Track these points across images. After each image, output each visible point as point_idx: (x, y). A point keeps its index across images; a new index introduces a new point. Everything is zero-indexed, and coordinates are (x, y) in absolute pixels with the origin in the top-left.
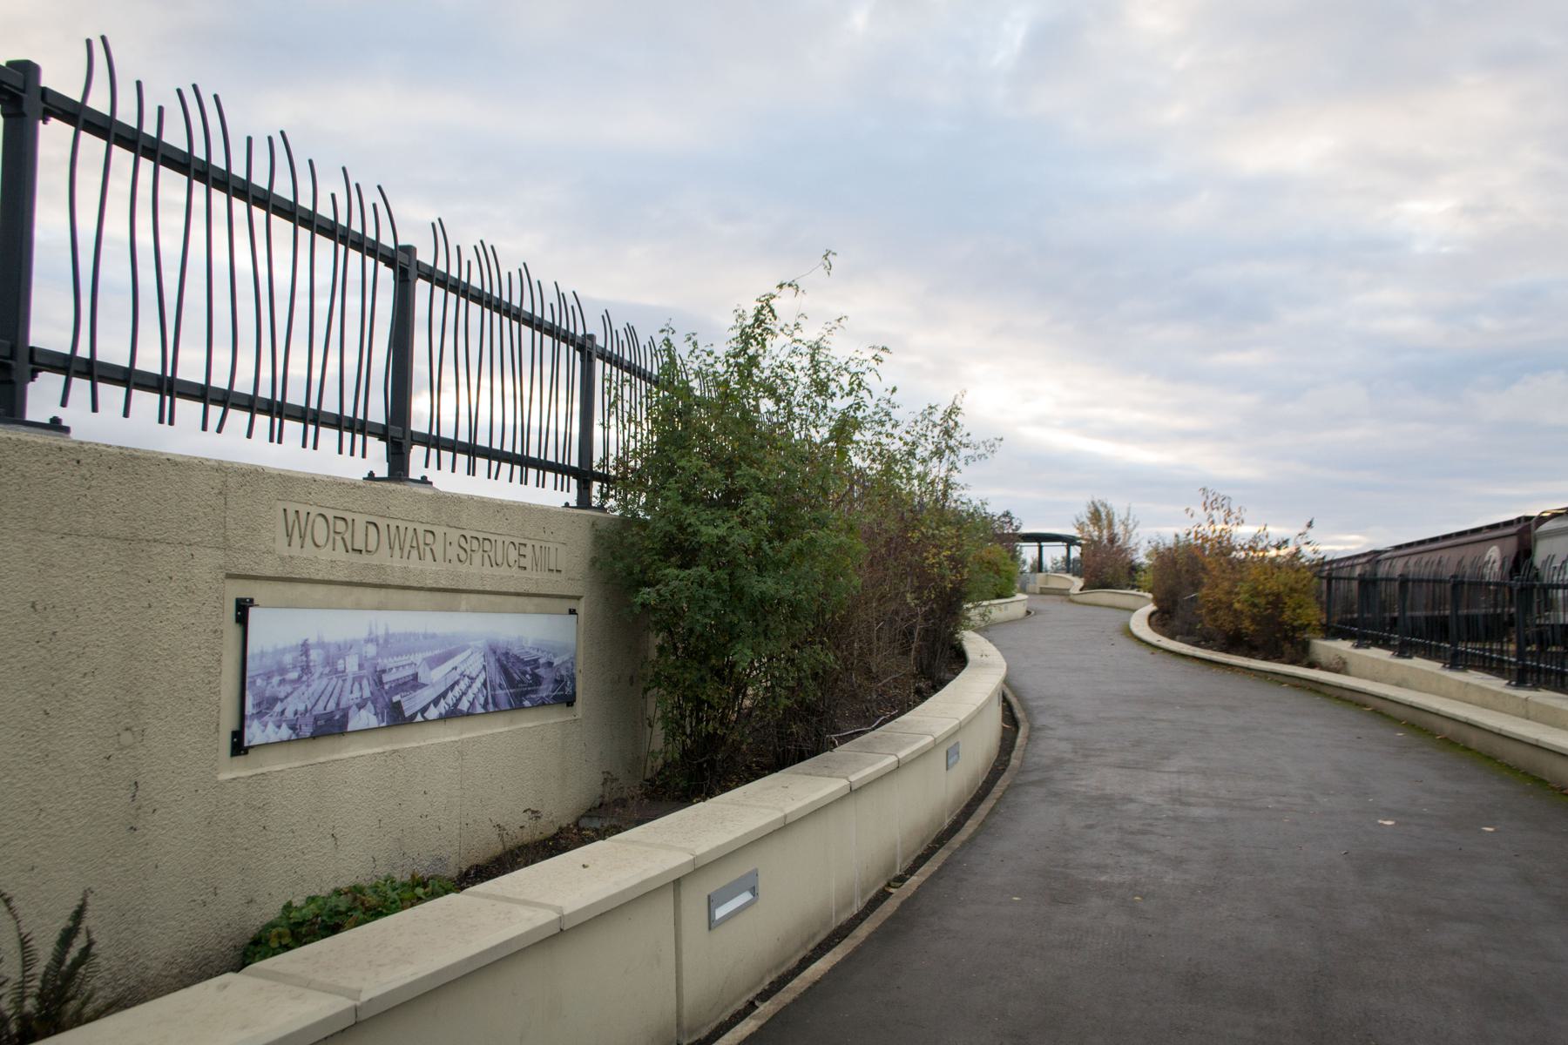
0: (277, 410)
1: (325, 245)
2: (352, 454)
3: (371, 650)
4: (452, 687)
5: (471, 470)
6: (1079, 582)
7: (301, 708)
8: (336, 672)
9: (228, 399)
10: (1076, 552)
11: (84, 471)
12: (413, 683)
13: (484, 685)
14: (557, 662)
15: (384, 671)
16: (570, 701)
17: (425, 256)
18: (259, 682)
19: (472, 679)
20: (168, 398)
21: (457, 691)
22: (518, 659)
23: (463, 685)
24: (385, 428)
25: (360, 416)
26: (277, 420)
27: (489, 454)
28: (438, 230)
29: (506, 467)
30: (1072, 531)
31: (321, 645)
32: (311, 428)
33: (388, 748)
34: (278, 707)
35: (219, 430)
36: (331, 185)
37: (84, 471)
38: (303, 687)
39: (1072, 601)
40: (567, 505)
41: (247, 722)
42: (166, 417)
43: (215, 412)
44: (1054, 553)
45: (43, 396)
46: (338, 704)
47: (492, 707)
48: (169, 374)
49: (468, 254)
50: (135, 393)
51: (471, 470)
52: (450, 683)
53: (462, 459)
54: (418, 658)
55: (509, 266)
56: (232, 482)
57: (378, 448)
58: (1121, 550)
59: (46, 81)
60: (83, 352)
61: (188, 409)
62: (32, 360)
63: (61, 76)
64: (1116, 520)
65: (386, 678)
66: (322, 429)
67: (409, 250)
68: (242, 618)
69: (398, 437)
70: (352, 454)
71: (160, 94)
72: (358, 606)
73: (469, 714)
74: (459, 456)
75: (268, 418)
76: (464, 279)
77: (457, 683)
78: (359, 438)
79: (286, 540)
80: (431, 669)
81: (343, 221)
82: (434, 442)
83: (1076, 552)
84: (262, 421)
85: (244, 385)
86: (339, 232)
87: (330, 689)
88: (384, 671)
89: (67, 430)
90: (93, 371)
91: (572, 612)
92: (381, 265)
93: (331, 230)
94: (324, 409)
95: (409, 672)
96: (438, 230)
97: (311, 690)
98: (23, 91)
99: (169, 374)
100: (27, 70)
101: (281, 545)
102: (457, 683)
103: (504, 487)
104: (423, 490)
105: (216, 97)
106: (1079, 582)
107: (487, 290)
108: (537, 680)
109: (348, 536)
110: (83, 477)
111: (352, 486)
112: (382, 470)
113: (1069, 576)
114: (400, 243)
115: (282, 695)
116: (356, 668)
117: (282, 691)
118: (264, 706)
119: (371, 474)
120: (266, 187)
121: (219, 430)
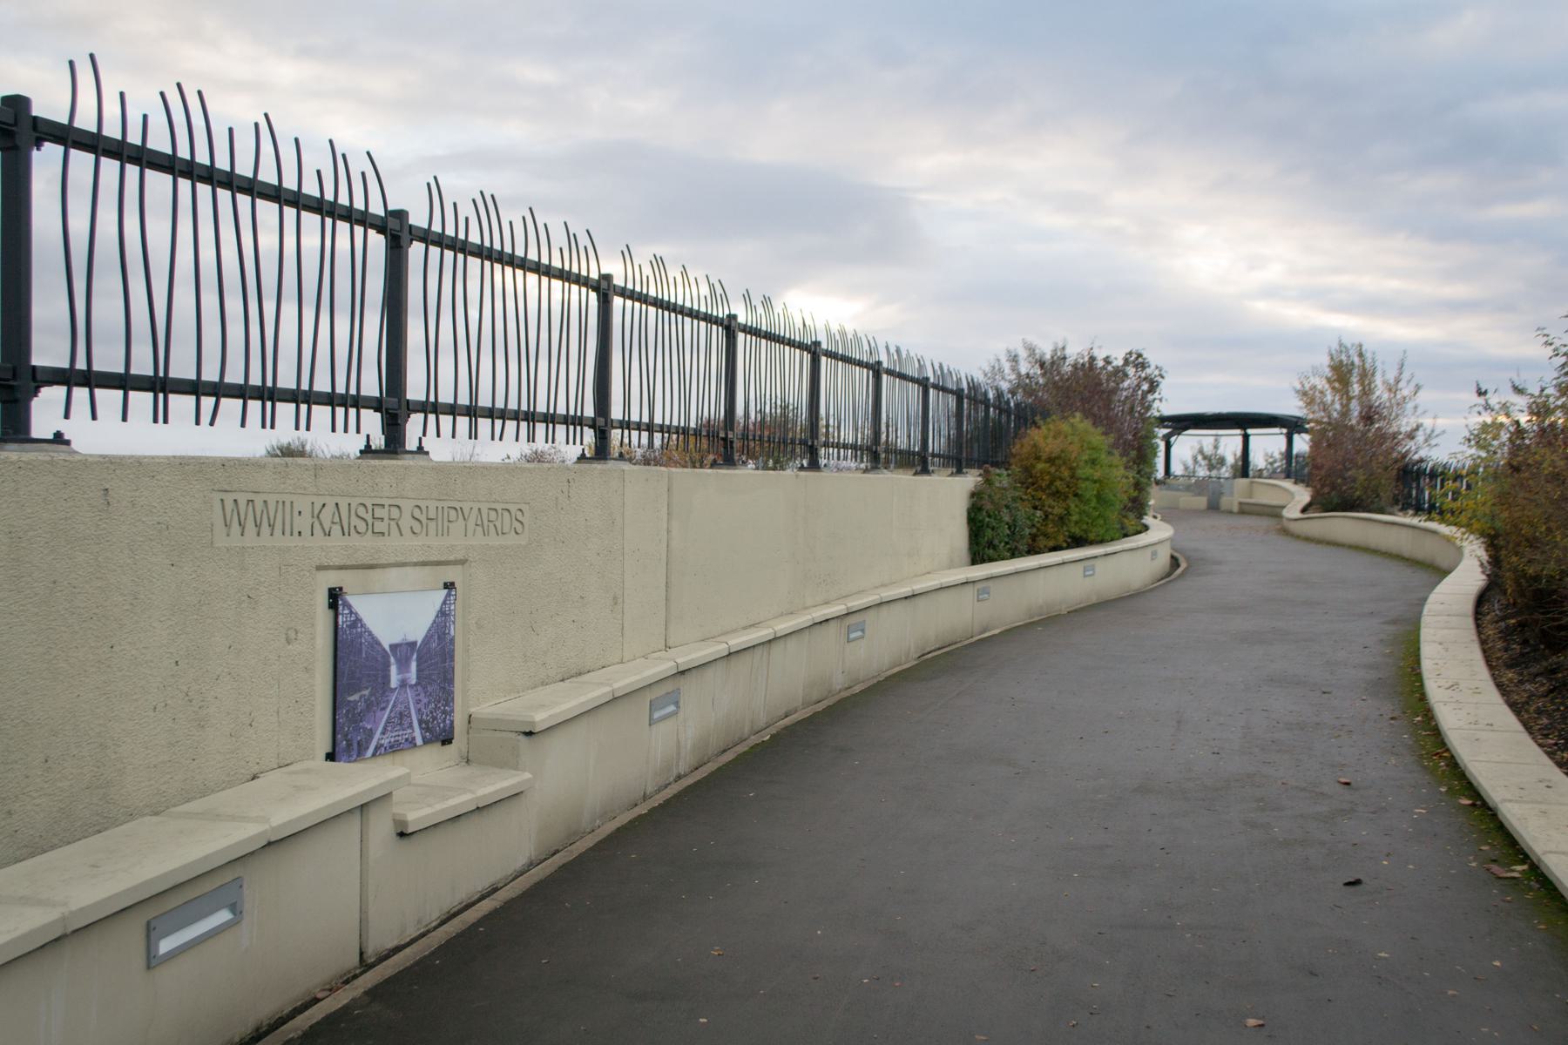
0: (269, 395)
1: (311, 220)
2: (346, 431)
5: (473, 434)
6: (1303, 495)
10: (1302, 444)
17: (418, 219)
20: (161, 396)
24: (594, 420)
25: (432, 399)
27: (491, 413)
28: (434, 190)
29: (511, 425)
30: (1292, 407)
32: (304, 407)
35: (212, 424)
36: (316, 159)
39: (1285, 532)
43: (208, 402)
44: (1267, 446)
45: (46, 411)
48: (161, 374)
49: (466, 210)
50: (132, 394)
51: (473, 434)
53: (463, 422)
55: (512, 214)
57: (372, 422)
58: (1382, 437)
59: (37, 111)
60: (81, 365)
62: (34, 378)
63: (49, 105)
64: (1378, 380)
66: (314, 407)
67: (401, 215)
70: (346, 431)
74: (459, 418)
75: (259, 403)
76: (462, 236)
78: (352, 411)
79: (255, 530)
81: (329, 196)
82: (431, 408)
83: (1302, 444)
84: (254, 406)
85: (234, 377)
86: (326, 208)
89: (68, 443)
92: (372, 233)
93: (319, 207)
94: (363, 393)
96: (434, 190)
98: (15, 124)
99: (161, 374)
100: (18, 103)
104: (58, 453)
105: (200, 93)
106: (1303, 495)
107: (487, 244)
112: (379, 441)
113: (1288, 484)
114: (390, 208)
120: (208, 163)
121: (212, 424)
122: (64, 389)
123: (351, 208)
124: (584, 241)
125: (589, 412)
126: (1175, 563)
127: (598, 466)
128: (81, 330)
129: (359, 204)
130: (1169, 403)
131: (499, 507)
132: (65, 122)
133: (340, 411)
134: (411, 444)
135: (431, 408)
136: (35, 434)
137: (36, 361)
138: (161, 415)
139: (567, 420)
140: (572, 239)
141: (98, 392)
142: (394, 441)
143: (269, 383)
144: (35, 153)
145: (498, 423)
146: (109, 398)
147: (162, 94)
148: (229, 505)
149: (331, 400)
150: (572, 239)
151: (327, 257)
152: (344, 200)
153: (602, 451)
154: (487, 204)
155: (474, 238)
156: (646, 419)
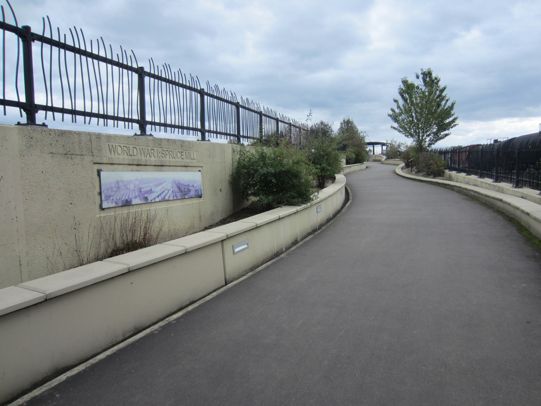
3: (137, 182)
4: (163, 192)
5: (183, 133)
6: (385, 157)
7: (118, 198)
13: (173, 192)
14: (195, 185)
17: (147, 69)
19: (169, 190)
21: (164, 194)
23: (166, 192)
29: (176, 130)
31: (122, 181)
34: (111, 198)
37: (52, 137)
42: (74, 121)
43: (88, 118)
53: (162, 128)
56: (93, 138)
57: (136, 126)
59: (33, 31)
65: (142, 190)
67: (142, 68)
69: (142, 123)
72: (132, 171)
73: (168, 200)
74: (48, 112)
89: (47, 126)
92: (134, 73)
95: (149, 188)
109: (128, 152)
112: (139, 132)
117: (112, 194)
123: (183, 84)
124: (195, 79)
125: (199, 127)
126: (367, 167)
127: (29, 127)
129: (184, 83)
130: (367, 141)
131: (168, 150)
132: (41, 34)
133: (127, 123)
134: (207, 139)
135: (209, 131)
136: (37, 123)
138: (166, 131)
139: (193, 129)
140: (192, 78)
141: (7, 107)
142: (203, 138)
148: (111, 147)
150: (192, 78)
154: (167, 67)
155: (164, 76)
156: (215, 130)
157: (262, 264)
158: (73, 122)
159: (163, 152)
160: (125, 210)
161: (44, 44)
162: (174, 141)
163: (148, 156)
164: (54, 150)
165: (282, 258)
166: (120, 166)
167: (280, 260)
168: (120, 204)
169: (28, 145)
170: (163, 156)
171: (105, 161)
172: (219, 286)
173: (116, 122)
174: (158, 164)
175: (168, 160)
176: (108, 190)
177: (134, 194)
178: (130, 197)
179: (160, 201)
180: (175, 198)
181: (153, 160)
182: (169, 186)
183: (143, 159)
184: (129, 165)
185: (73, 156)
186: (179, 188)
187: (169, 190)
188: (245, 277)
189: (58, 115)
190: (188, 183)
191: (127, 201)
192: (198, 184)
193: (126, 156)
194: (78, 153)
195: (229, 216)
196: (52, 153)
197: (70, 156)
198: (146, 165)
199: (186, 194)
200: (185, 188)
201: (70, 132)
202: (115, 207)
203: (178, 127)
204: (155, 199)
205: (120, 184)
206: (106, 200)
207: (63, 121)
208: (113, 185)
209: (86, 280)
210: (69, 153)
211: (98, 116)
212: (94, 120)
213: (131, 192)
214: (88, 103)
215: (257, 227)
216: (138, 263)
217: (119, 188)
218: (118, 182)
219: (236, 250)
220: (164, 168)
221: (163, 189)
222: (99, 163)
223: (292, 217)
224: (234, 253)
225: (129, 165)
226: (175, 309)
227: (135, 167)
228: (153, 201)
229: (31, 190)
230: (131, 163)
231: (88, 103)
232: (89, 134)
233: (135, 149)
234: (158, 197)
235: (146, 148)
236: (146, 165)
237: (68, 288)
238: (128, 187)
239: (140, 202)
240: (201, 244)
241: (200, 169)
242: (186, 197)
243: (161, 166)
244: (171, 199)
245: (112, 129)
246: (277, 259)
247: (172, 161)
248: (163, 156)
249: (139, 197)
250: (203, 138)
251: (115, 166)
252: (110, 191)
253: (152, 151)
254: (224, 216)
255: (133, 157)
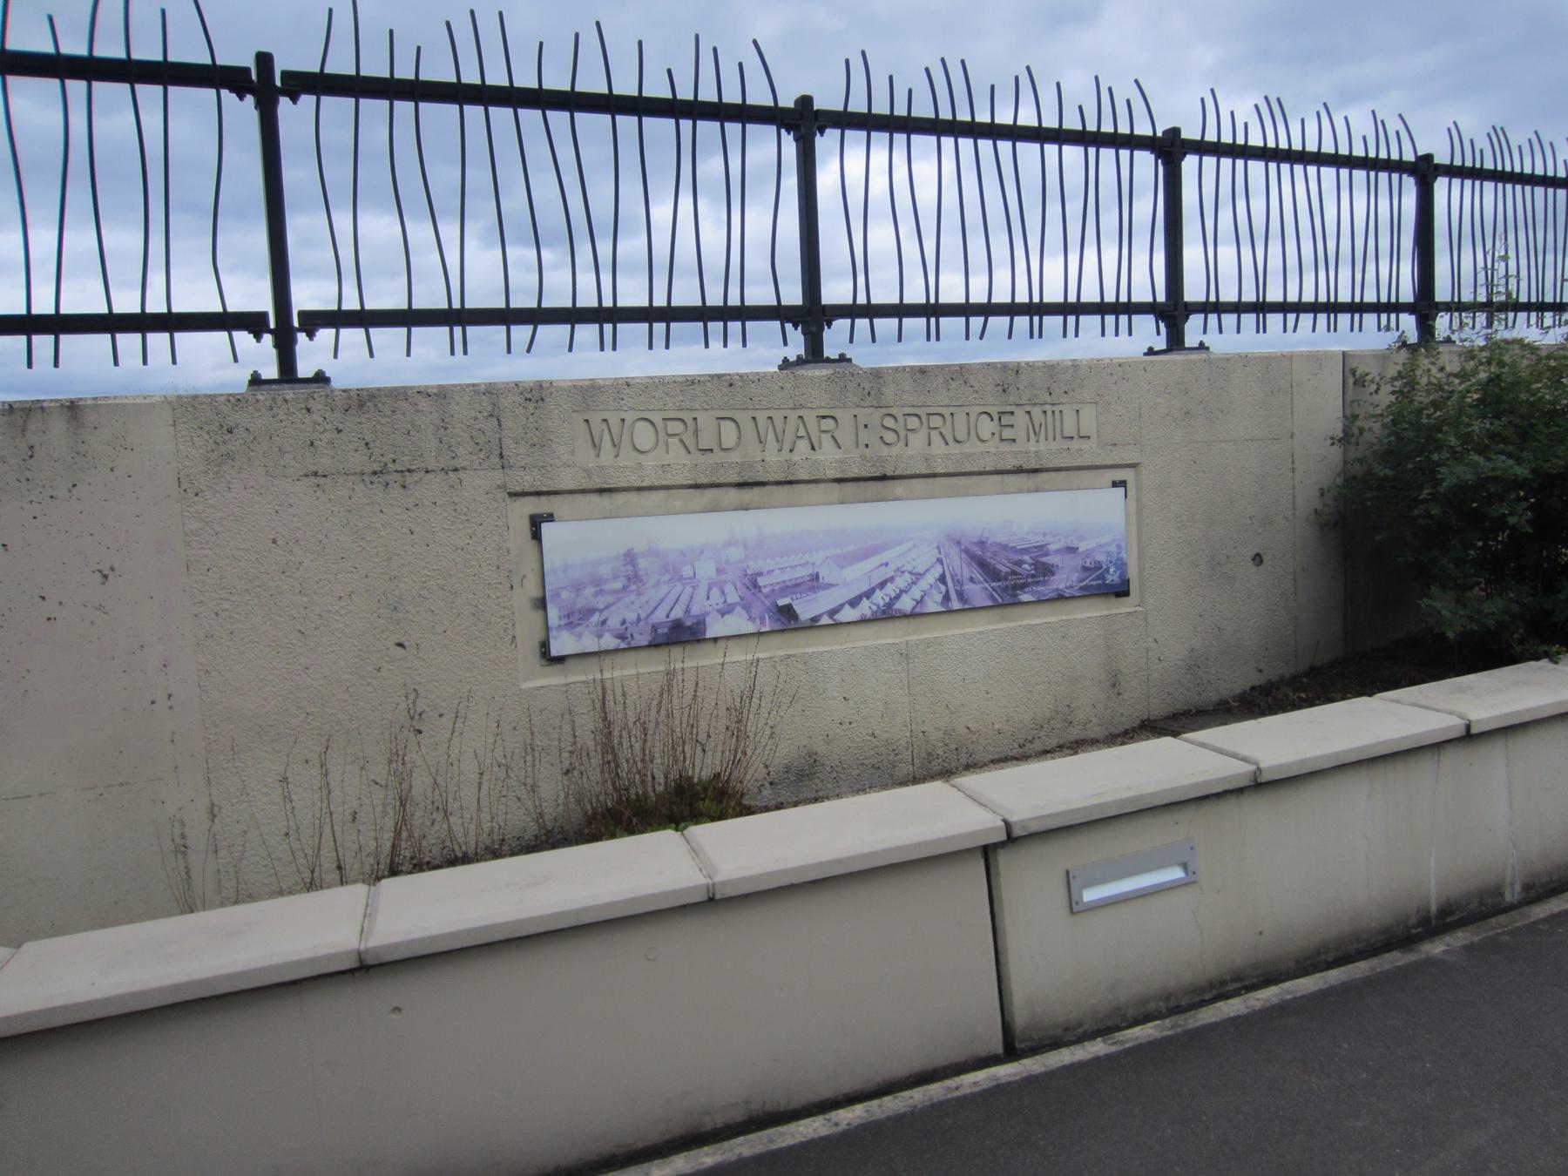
3: (736, 553)
4: (882, 585)
7: (632, 616)
8: (681, 578)
9: (1299, 308)
11: (317, 417)
12: (814, 583)
13: (942, 579)
14: (1083, 547)
15: (760, 574)
16: (1126, 593)
18: (564, 594)
19: (919, 576)
21: (890, 590)
22: (1004, 547)
23: (901, 582)
26: (933, 320)
31: (653, 553)
32: (1036, 319)
33: (781, 653)
34: (596, 618)
37: (317, 417)
38: (632, 597)
40: (256, 381)
41: (553, 634)
42: (1261, 328)
46: (687, 611)
47: (957, 605)
52: (876, 580)
54: (818, 557)
55: (1518, 138)
56: (505, 402)
57: (1408, 322)
59: (1184, 135)
61: (1274, 320)
65: (761, 581)
68: (536, 535)
69: (1172, 312)
71: (1245, 113)
72: (715, 508)
73: (913, 615)
77: (891, 579)
80: (842, 567)
84: (1322, 317)
87: (672, 597)
88: (760, 574)
89: (850, 360)
90: (1218, 308)
91: (1123, 484)
95: (805, 572)
97: (643, 599)
101: (585, 456)
102: (891, 579)
103: (691, 355)
108: (1044, 571)
109: (689, 438)
110: (315, 423)
111: (236, 401)
112: (1161, 343)
115: (601, 606)
116: (713, 573)
117: (601, 602)
118: (576, 616)
119: (785, 360)
122: (963, 319)
128: (1212, 275)
137: (1437, 299)
138: (1332, 328)
142: (1176, 341)
143: (932, 301)
144: (818, 138)
145: (1357, 316)
146: (1229, 319)
147: (943, 60)
149: (1377, 308)
151: (1091, 183)
152: (1283, 145)
153: (814, 351)
157: (1307, 965)
158: (1032, 336)
159: (889, 422)
160: (652, 666)
161: (138, 87)
162: (959, 374)
163: (803, 445)
164: (325, 463)
165: (1431, 962)
166: (645, 495)
167: (1416, 967)
168: (643, 640)
169: (214, 456)
170: (890, 437)
171: (567, 480)
172: (959, 1056)
173: (458, 330)
174: (855, 471)
175: (915, 450)
176: (578, 588)
177: (716, 598)
178: (695, 611)
179: (863, 621)
180: (956, 605)
181: (829, 458)
182: (923, 558)
183: (773, 461)
184: (696, 486)
185: (410, 478)
186: (983, 565)
187: (919, 576)
188: (1098, 1048)
189: (886, 325)
190: (1038, 540)
191: (677, 626)
192: (1104, 540)
193: (677, 456)
194: (432, 463)
195: (1313, 671)
196: (316, 474)
197: (398, 477)
198: (791, 483)
199: (1023, 587)
200: (1019, 563)
201: (399, 395)
202: (616, 651)
203: (1315, 308)
204: (832, 613)
205: (642, 563)
206: (570, 625)
207: (236, 360)
208: (605, 570)
209: (137, 987)
210: (392, 467)
211: (1011, 310)
212: (999, 323)
213: (702, 590)
214: (586, 280)
215: (1259, 785)
216: (435, 931)
217: (635, 578)
218: (630, 558)
219: (1090, 895)
220: (898, 488)
221: (887, 572)
222: (538, 494)
223: (1424, 768)
224: (1074, 907)
225: (696, 486)
226: (654, 1136)
227: (733, 495)
228: (825, 620)
229: (226, 605)
230: (705, 480)
231: (586, 280)
232: (491, 391)
233: (727, 426)
234: (854, 603)
235: (793, 416)
236: (791, 483)
237: (53, 1010)
238: (687, 571)
239: (750, 627)
240: (469, 932)
241: (1120, 475)
242: (1025, 597)
243: (878, 480)
244: (931, 606)
245: (1092, 342)
246: (1396, 959)
247: (943, 455)
248: (890, 437)
249: (747, 608)
250: (1176, 341)
251: (620, 498)
252: (589, 591)
253: (828, 424)
254: (1272, 673)
255: (719, 457)
